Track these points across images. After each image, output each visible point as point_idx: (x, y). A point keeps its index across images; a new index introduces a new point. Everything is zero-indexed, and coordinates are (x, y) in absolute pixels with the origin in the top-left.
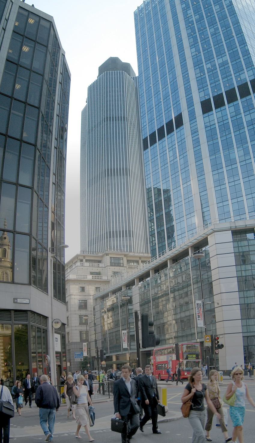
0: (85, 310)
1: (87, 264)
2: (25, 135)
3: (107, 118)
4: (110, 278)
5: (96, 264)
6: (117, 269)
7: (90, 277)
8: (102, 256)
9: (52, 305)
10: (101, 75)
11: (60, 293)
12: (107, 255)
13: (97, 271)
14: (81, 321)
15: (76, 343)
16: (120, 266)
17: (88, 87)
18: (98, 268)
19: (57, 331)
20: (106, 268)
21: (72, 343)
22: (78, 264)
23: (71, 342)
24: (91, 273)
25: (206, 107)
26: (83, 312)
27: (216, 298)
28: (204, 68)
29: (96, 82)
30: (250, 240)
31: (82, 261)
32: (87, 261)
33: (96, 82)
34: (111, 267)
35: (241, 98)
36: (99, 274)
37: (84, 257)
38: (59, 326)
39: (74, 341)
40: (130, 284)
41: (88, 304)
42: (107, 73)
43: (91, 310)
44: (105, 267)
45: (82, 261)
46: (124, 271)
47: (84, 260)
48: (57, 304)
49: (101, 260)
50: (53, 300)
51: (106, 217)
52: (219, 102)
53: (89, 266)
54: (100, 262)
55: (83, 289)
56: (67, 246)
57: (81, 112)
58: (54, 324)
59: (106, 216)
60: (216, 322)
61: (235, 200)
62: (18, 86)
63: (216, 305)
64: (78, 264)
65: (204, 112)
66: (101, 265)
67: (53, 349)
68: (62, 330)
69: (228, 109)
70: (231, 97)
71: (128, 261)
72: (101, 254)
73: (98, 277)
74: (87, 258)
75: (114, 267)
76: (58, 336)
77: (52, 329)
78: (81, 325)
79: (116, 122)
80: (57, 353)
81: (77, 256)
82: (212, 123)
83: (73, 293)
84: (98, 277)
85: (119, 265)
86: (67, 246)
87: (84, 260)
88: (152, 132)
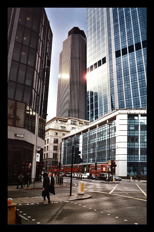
1: (60, 122)
2: (29, 63)
4: (70, 130)
5: (64, 123)
6: (74, 126)
7: (60, 129)
8: (67, 120)
9: (37, 139)
11: (42, 134)
12: (70, 119)
16: (75, 125)
19: (38, 152)
22: (55, 121)
25: (118, 54)
26: (56, 145)
27: (117, 145)
30: (136, 120)
31: (57, 120)
32: (59, 121)
35: (136, 51)
37: (58, 119)
38: (39, 149)
40: (79, 134)
41: (59, 141)
42: (72, 35)
45: (57, 120)
46: (77, 128)
47: (58, 120)
48: (40, 139)
50: (38, 137)
52: (124, 52)
54: (66, 122)
55: (57, 134)
56: (47, 115)
58: (37, 148)
60: (115, 155)
61: (128, 99)
62: (25, 39)
63: (116, 147)
64: (55, 121)
65: (116, 57)
66: (66, 123)
67: (35, 160)
68: (41, 152)
69: (128, 56)
70: (131, 49)
71: (79, 123)
72: (67, 119)
75: (72, 125)
76: (39, 155)
77: (36, 151)
80: (37, 162)
81: (55, 118)
82: (126, 60)
83: (50, 136)
85: (75, 124)
86: (47, 115)
87: (58, 120)
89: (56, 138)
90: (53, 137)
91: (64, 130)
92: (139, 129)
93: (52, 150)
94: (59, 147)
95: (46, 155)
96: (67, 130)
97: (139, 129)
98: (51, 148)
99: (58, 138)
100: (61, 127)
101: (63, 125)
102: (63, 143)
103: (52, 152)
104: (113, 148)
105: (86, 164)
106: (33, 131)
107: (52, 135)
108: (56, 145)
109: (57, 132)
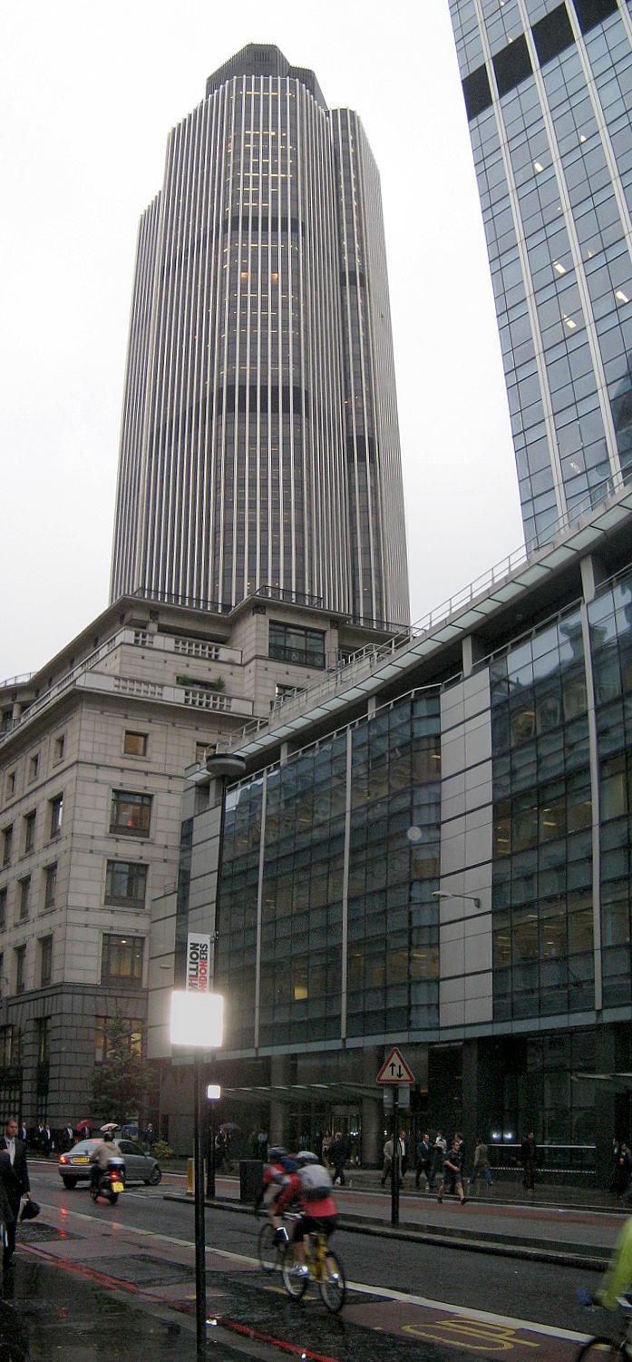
0: (141, 839)
1: (167, 642)
3: (235, 220)
4: (262, 710)
7: (175, 696)
10: (218, 89)
13: (210, 677)
14: (112, 891)
15: (84, 986)
17: (170, 131)
18: (213, 665)
20: (248, 667)
21: (61, 985)
23: (56, 979)
24: (183, 681)
26: (129, 849)
28: (568, 237)
29: (201, 111)
32: (164, 630)
33: (201, 111)
34: (273, 665)
36: (217, 686)
39: (74, 976)
43: (165, 843)
44: (240, 665)
47: (153, 627)
49: (229, 638)
51: (216, 556)
53: (173, 650)
54: (224, 641)
57: (139, 219)
59: (216, 549)
66: (224, 653)
73: (211, 700)
74: (164, 621)
78: (111, 907)
79: (275, 216)
84: (211, 700)
88: (546, 14)
89: (134, 783)
90: (103, 775)
91: (206, 710)
92: (248, 372)
93: (97, 900)
94: (160, 879)
95: (33, 955)
96: (237, 707)
97: (248, 372)
98: (86, 885)
99: (152, 784)
100: (183, 681)
101: (200, 669)
102: (208, 825)
103: (94, 918)
104: (425, 921)
105: (587, 1019)
106: (288, 754)
107: (97, 759)
108: (129, 849)
109: (142, 727)
